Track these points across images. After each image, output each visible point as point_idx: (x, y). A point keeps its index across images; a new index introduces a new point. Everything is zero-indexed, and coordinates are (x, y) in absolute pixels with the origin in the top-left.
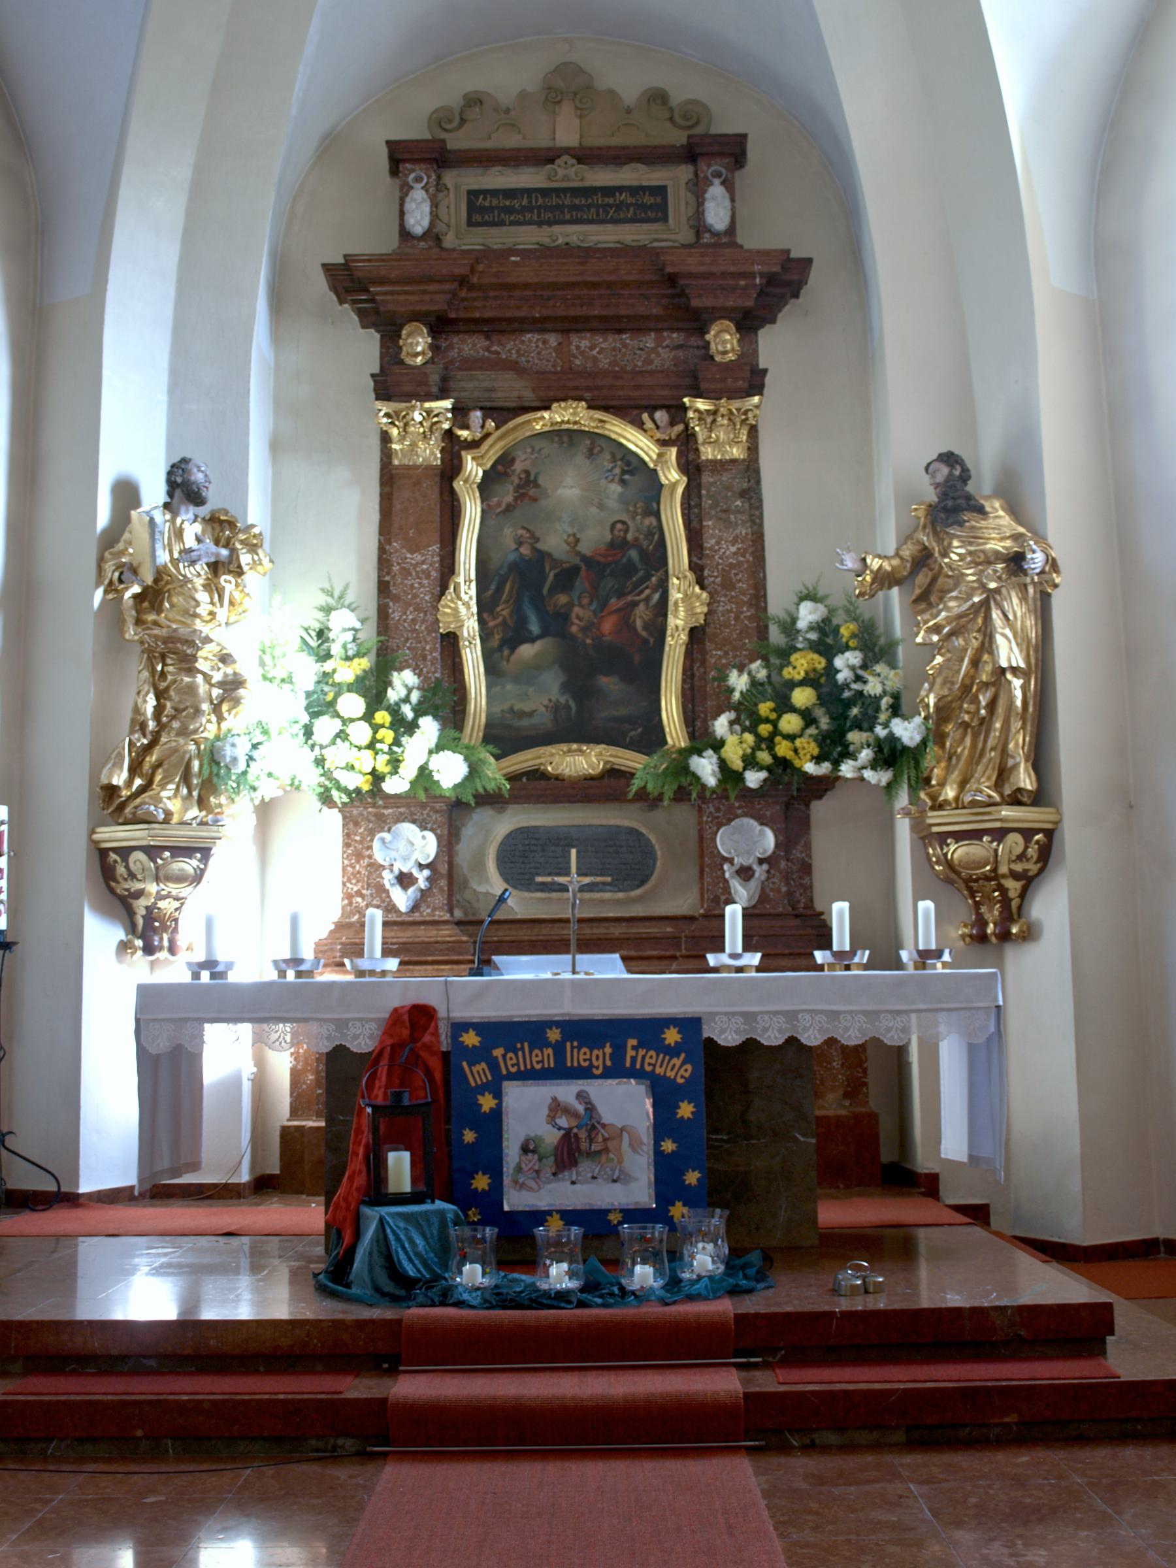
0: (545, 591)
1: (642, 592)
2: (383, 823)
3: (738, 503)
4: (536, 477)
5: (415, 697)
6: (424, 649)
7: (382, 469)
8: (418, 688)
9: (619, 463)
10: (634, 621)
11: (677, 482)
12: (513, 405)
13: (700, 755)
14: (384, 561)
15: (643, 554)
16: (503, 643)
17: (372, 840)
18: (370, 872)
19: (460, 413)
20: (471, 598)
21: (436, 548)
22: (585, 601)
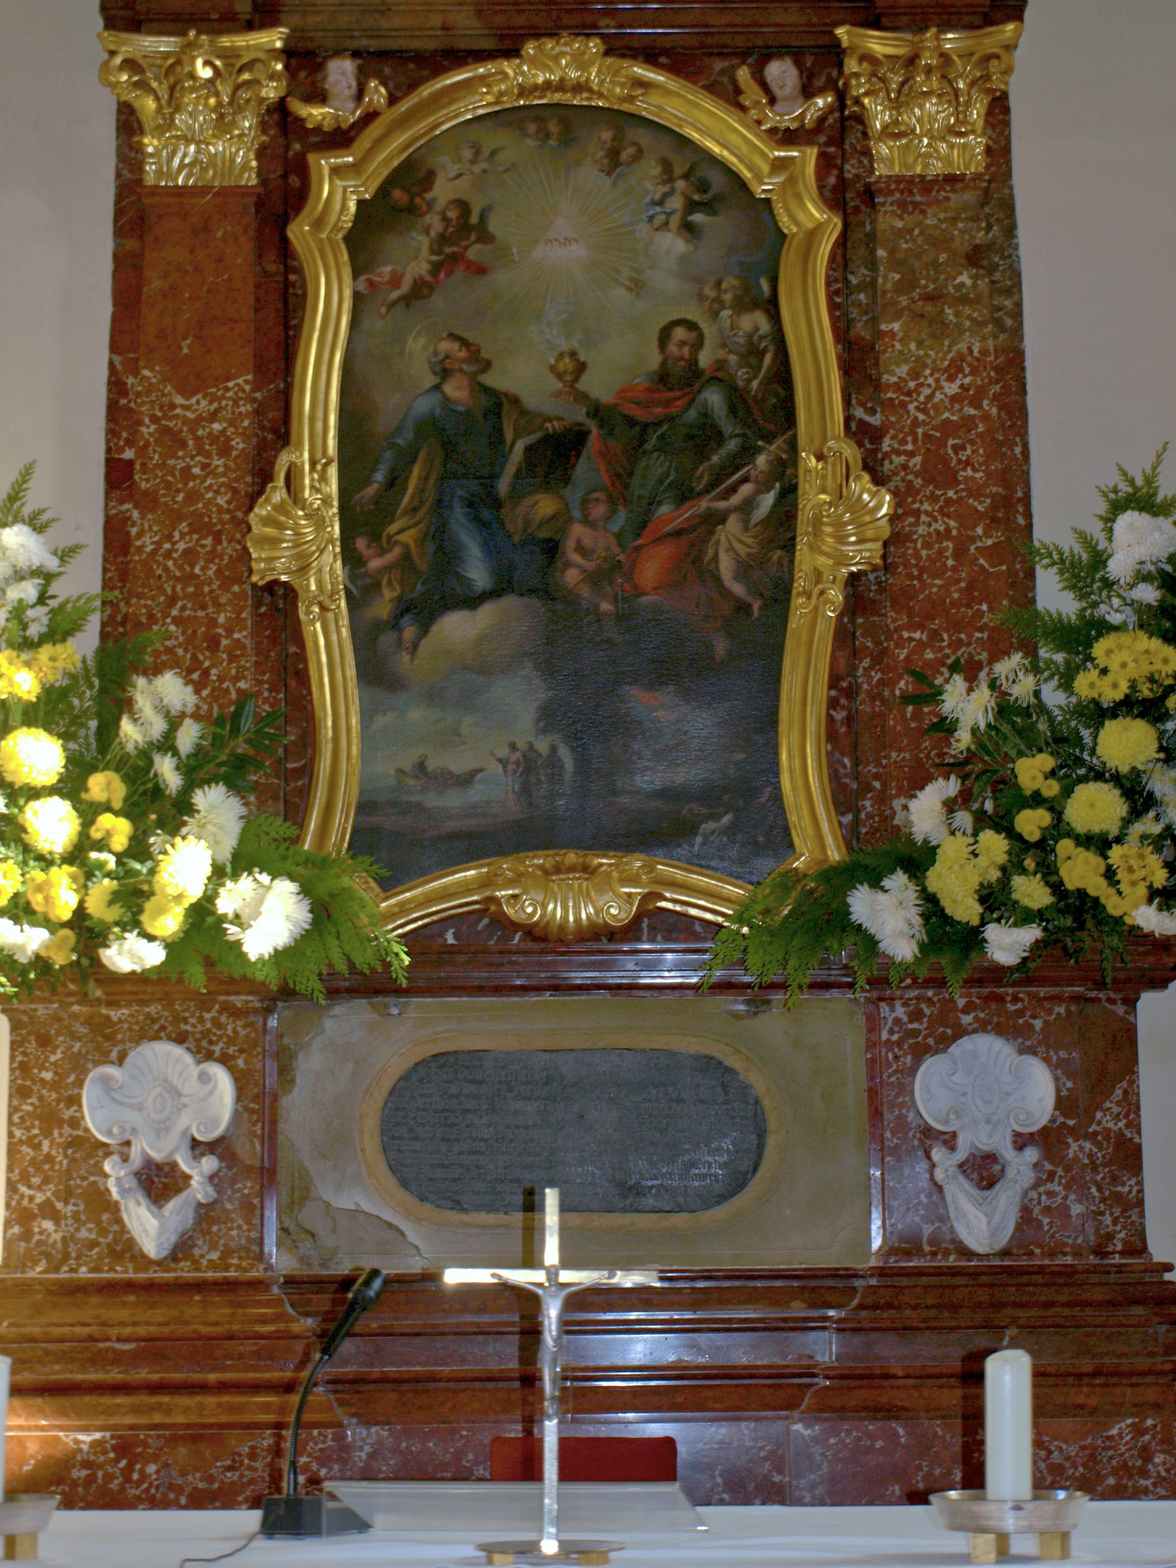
0: (503, 486)
1: (734, 489)
2: (108, 1043)
3: (964, 278)
4: (483, 217)
5: (188, 736)
6: (213, 622)
7: (119, 197)
8: (196, 716)
9: (681, 184)
10: (716, 559)
11: (818, 229)
12: (431, 45)
13: (876, 883)
14: (119, 413)
15: (737, 400)
16: (405, 608)
17: (79, 1083)
18: (73, 1161)
19: (303, 60)
20: (326, 501)
21: (243, 381)
22: (599, 511)
